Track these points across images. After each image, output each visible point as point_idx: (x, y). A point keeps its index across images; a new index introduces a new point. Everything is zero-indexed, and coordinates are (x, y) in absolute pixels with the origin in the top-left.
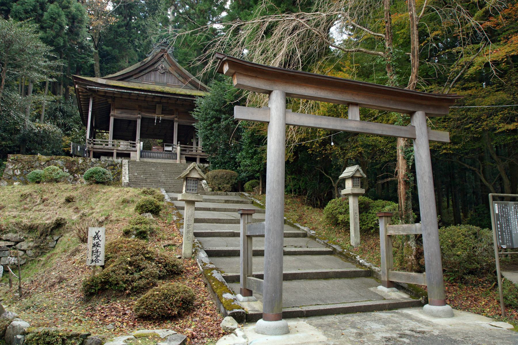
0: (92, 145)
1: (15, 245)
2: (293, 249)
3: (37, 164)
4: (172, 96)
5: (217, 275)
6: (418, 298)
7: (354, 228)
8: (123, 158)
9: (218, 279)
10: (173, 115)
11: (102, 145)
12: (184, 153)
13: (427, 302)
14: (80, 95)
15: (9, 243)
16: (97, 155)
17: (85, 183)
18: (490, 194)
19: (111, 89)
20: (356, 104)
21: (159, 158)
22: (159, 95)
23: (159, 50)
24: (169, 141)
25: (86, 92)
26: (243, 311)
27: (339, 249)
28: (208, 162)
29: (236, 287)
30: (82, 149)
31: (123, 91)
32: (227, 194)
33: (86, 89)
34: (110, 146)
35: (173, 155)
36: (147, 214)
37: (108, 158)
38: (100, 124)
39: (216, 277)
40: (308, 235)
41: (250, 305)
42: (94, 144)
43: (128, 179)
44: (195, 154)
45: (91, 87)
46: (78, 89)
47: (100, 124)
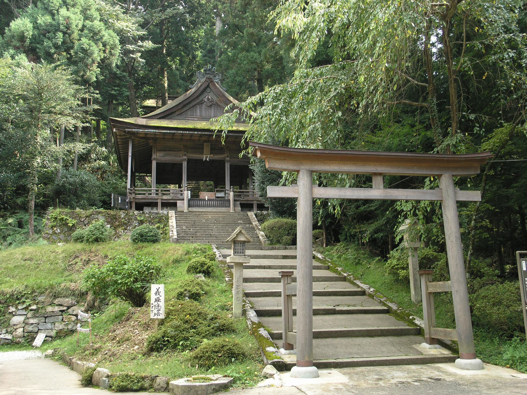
0: (133, 195)
2: (346, 308)
5: (263, 332)
6: (454, 352)
7: (414, 284)
8: (169, 208)
9: (264, 335)
11: (144, 194)
15: (62, 308)
16: (140, 207)
17: (130, 240)
18: (517, 252)
19: (152, 131)
22: (206, 133)
23: (204, 79)
25: (124, 135)
27: (394, 307)
28: (267, 209)
29: (280, 343)
32: (286, 249)
33: (125, 132)
34: (154, 196)
38: (142, 166)
40: (367, 293)
41: (287, 357)
42: (136, 194)
44: (251, 199)
46: (115, 133)
47: (142, 166)
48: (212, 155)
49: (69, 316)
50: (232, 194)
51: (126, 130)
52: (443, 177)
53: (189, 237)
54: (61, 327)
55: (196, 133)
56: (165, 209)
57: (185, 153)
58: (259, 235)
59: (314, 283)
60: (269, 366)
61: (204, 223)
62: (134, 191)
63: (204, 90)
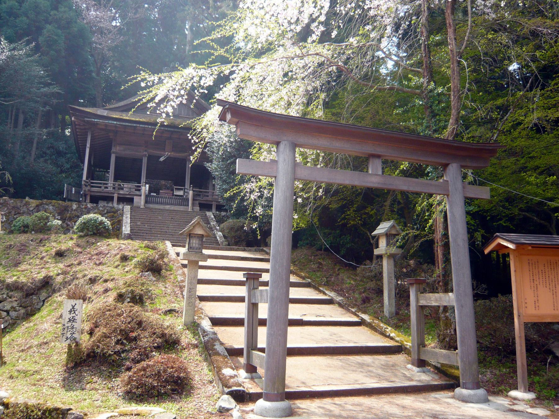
3: (24, 209)
8: (125, 203)
11: (100, 187)
12: (197, 198)
13: (458, 386)
20: (378, 156)
21: (168, 204)
24: (180, 183)
26: (243, 389)
30: (78, 192)
33: (84, 121)
34: (110, 189)
35: (184, 201)
36: (147, 273)
37: (108, 203)
39: (218, 349)
42: (92, 187)
43: (129, 229)
44: (210, 199)
45: (90, 120)
50: (191, 193)
52: (450, 167)
56: (121, 203)
59: (290, 288)
60: (226, 397)
61: (160, 220)
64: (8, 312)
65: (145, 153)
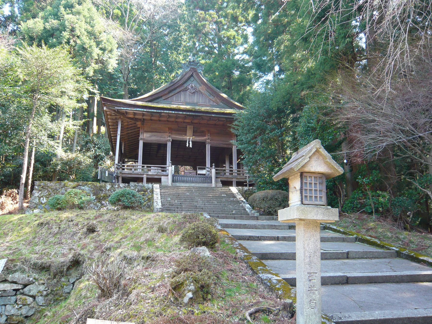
1: (22, 289)
4: (205, 115)
8: (153, 183)
10: (205, 136)
11: (131, 169)
14: (110, 129)
15: (15, 287)
16: (126, 180)
19: (140, 110)
22: (190, 113)
23: (189, 69)
31: (153, 111)
33: (114, 111)
34: (139, 171)
43: (160, 204)
45: (120, 108)
47: (128, 154)
48: (194, 137)
49: (24, 297)
50: (213, 171)
51: (116, 108)
53: (174, 208)
54: (13, 312)
55: (181, 113)
56: (150, 183)
57: (170, 135)
58: (246, 208)
62: (121, 166)
63: (189, 78)
64: (34, 297)
65: (169, 138)
